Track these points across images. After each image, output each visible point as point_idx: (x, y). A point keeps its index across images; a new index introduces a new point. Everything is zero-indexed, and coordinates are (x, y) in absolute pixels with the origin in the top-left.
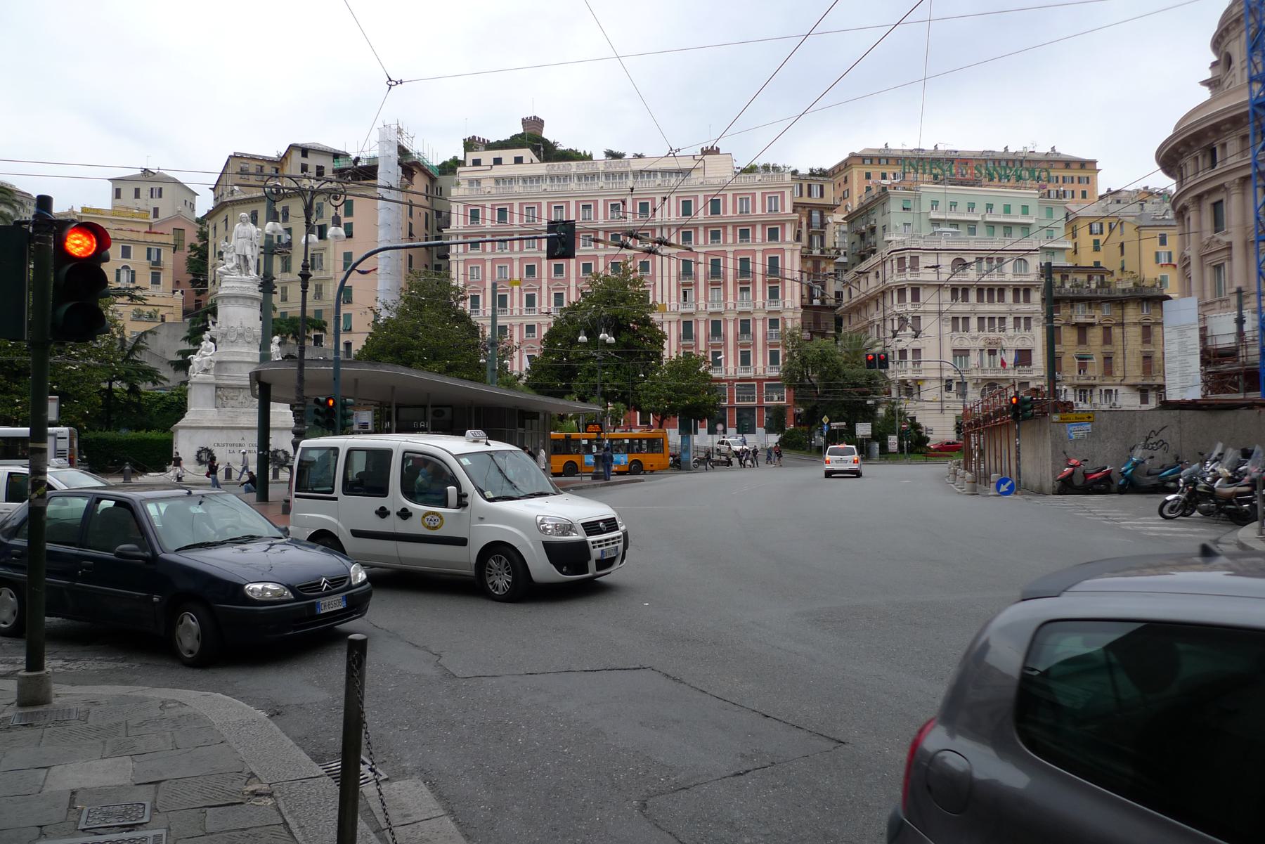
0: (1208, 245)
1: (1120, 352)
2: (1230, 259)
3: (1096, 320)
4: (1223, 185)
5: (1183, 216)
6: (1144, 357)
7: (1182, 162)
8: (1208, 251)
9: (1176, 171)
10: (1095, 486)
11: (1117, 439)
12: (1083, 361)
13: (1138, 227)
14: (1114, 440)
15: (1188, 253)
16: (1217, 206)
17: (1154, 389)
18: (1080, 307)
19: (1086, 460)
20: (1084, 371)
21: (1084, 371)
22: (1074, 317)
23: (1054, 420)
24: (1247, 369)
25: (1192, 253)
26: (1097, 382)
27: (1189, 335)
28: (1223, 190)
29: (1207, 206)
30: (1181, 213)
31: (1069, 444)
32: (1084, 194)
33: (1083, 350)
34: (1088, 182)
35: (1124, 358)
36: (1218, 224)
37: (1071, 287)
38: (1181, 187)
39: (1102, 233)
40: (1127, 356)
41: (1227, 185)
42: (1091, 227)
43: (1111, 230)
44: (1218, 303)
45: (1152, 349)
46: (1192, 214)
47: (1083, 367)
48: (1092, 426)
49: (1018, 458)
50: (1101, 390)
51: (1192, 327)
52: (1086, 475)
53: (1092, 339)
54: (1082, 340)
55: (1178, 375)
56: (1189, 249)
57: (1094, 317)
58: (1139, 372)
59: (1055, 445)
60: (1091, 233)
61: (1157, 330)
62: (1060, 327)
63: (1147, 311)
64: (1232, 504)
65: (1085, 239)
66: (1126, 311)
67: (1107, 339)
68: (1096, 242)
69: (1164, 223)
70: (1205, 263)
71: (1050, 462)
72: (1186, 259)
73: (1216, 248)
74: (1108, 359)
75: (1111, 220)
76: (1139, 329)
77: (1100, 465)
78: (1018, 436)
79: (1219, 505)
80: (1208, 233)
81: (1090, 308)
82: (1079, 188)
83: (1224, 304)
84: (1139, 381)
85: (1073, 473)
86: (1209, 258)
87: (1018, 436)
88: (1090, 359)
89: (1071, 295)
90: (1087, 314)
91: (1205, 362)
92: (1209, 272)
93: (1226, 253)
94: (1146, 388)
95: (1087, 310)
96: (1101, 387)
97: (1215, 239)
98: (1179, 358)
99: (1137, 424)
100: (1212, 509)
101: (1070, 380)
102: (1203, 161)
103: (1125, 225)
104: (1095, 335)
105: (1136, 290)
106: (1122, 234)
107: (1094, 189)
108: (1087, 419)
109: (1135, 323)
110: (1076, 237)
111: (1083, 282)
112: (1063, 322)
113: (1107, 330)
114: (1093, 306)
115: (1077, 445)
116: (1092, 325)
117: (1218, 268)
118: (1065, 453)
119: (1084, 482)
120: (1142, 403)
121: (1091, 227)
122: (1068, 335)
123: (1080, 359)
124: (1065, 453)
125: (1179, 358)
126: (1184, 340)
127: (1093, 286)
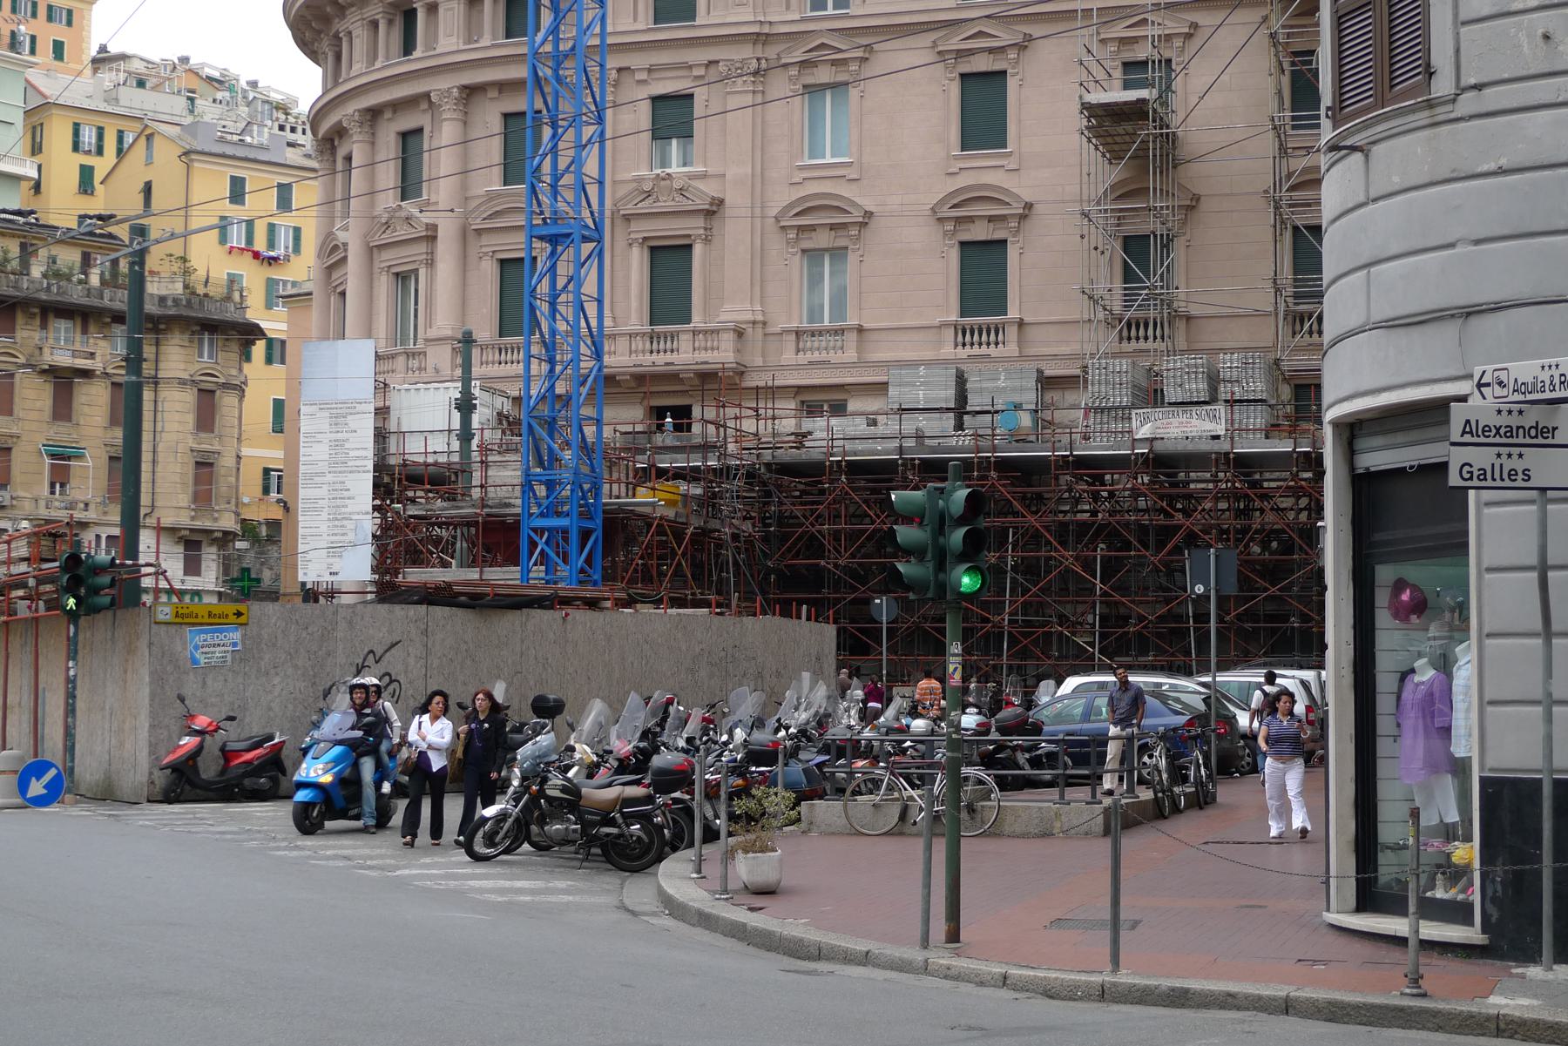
0: (387, 225)
2: (431, 263)
3: (96, 365)
4: (427, 95)
5: (333, 150)
6: (197, 463)
7: (340, 26)
8: (388, 237)
9: (325, 46)
10: (247, 782)
11: (296, 667)
12: (62, 462)
13: (185, 154)
14: (290, 671)
15: (342, 236)
16: (410, 137)
17: (214, 541)
18: (61, 328)
19: (232, 719)
20: (62, 485)
21: (62, 485)
22: (46, 351)
23: (161, 617)
24: (489, 515)
25: (352, 237)
26: (91, 515)
27: (353, 425)
28: (424, 106)
29: (389, 135)
30: (330, 141)
31: (191, 676)
32: (58, 49)
33: (62, 434)
34: (69, 23)
36: (409, 186)
37: (45, 276)
38: (336, 84)
39: (100, 151)
40: (161, 457)
41: (434, 98)
42: (76, 133)
43: (120, 152)
44: (401, 360)
45: (217, 447)
46: (357, 148)
47: (60, 478)
48: (244, 636)
49: (70, 710)
50: (98, 537)
51: (360, 408)
52: (227, 754)
53: (86, 409)
54: (63, 409)
55: (325, 516)
56: (345, 228)
57: (92, 355)
58: (184, 499)
59: (158, 679)
60: (76, 147)
61: (227, 401)
62: (213, 392)
63: (210, 357)
64: (612, 822)
65: (63, 165)
66: (162, 348)
68: (86, 173)
69: (240, 152)
70: (377, 265)
71: (144, 722)
72: (336, 247)
73: (402, 232)
75: (122, 124)
76: (189, 397)
77: (257, 730)
78: (72, 654)
79: (586, 825)
80: (388, 200)
81: (85, 331)
82: (48, 33)
83: (414, 363)
84: (184, 519)
85: (199, 749)
86: (387, 255)
87: (72, 654)
88: (80, 457)
89: (44, 296)
90: (78, 346)
91: (381, 489)
92: (384, 285)
93: (422, 248)
94: (195, 537)
95: (78, 337)
96: (98, 530)
97: (403, 214)
98: (329, 478)
99: (340, 635)
100: (572, 836)
101: (28, 506)
102: (388, 34)
103: (157, 140)
104: (94, 402)
105: (189, 302)
106: (149, 162)
107: (81, 40)
108: (233, 618)
109: (182, 382)
110: (40, 151)
111: (71, 269)
112: (22, 360)
114: (92, 328)
115: (209, 682)
116: (86, 374)
117: (403, 278)
118: (182, 700)
119: (223, 772)
120: (186, 573)
121: (76, 133)
122: (30, 394)
123: (53, 456)
124: (182, 700)
125: (329, 478)
127: (95, 280)
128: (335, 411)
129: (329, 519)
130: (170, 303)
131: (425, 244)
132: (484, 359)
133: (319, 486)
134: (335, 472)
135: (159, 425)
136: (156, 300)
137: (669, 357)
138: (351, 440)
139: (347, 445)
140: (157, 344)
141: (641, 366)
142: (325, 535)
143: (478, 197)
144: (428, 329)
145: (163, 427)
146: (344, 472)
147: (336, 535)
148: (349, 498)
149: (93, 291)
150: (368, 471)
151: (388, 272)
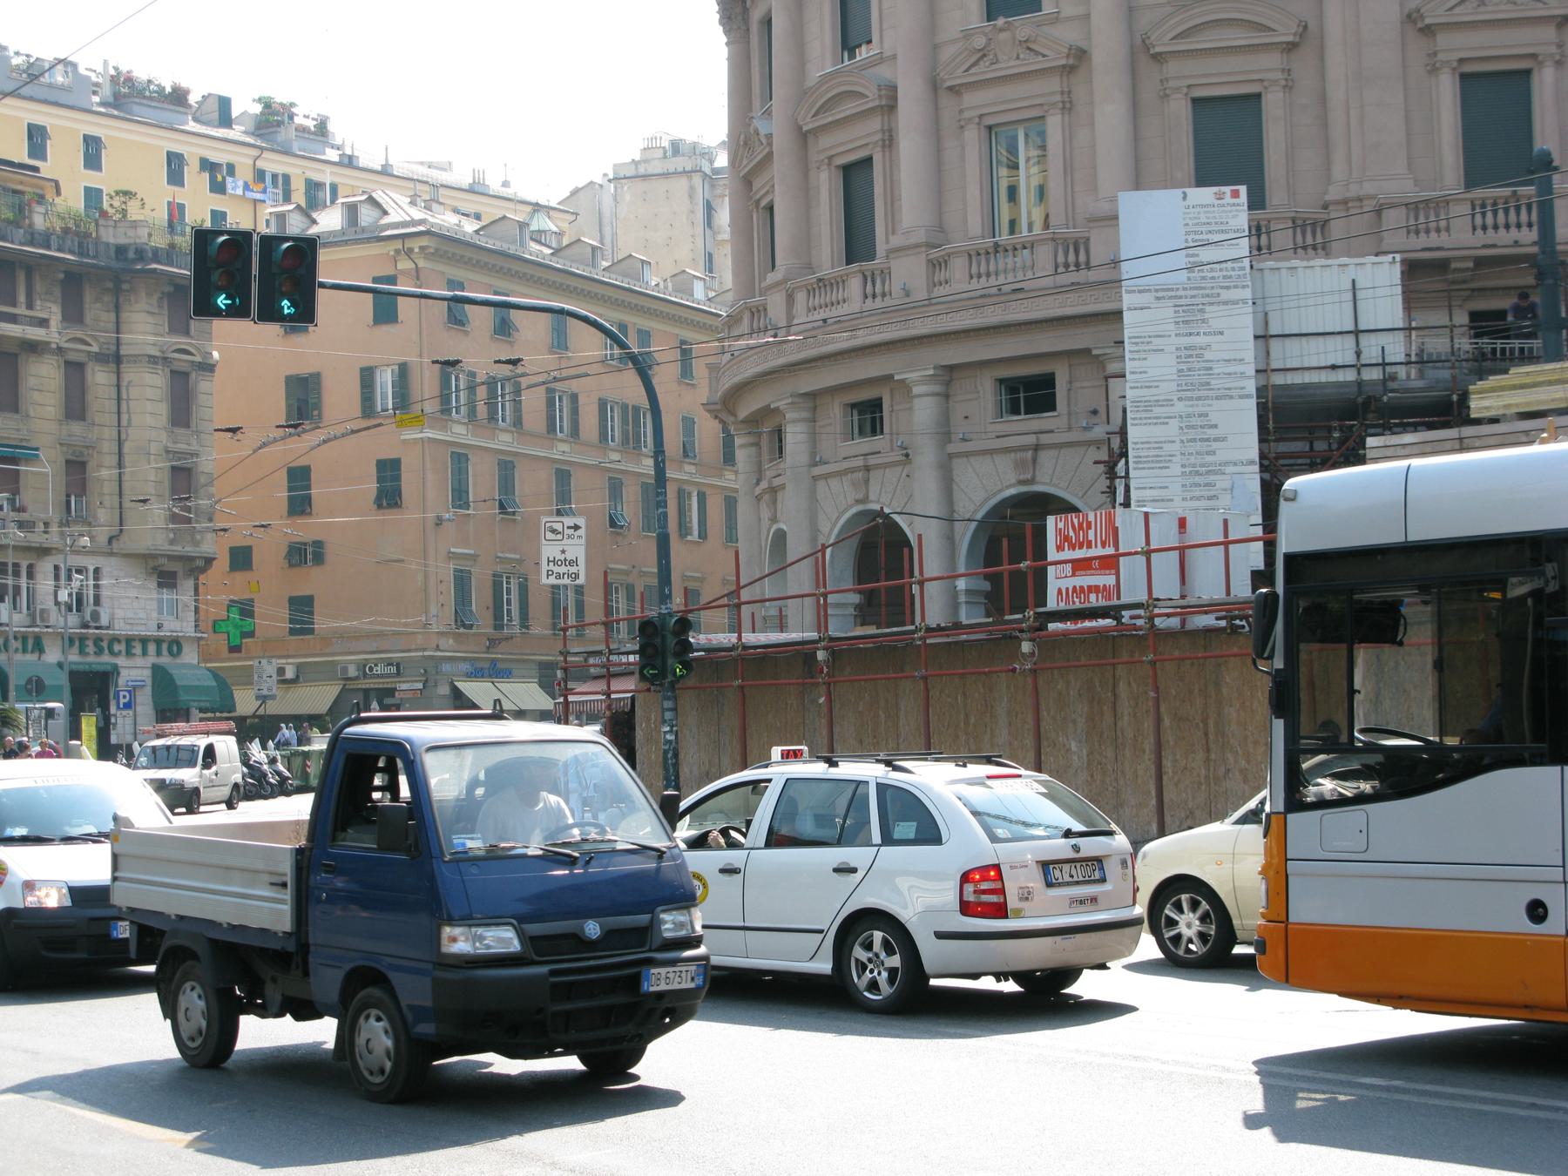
1: (109, 447)
2: (889, 141)
6: (174, 468)
27: (1215, 324)
35: (120, 465)
40: (127, 460)
45: (194, 447)
53: (36, 396)
55: (1176, 469)
66: (124, 315)
67: (75, 406)
73: (848, 108)
74: (76, 470)
86: (826, 141)
88: (32, 459)
98: (1180, 407)
109: (153, 360)
113: (75, 371)
116: (33, 347)
125: (1180, 407)
126: (1201, 340)
128: (1183, 302)
129: (1183, 474)
130: (131, 255)
131: (1058, 79)
132: (974, 270)
133: (1163, 421)
134: (1191, 399)
135: (125, 417)
136: (113, 250)
137: (1434, 239)
138: (1214, 347)
139: (1208, 355)
140: (117, 309)
141: (1494, 246)
142: (1178, 500)
143: (953, 42)
144: (891, 238)
145: (129, 420)
146: (1206, 398)
147: (1198, 498)
148: (1216, 440)
149: (36, 236)
150: (1248, 396)
151: (979, 124)
